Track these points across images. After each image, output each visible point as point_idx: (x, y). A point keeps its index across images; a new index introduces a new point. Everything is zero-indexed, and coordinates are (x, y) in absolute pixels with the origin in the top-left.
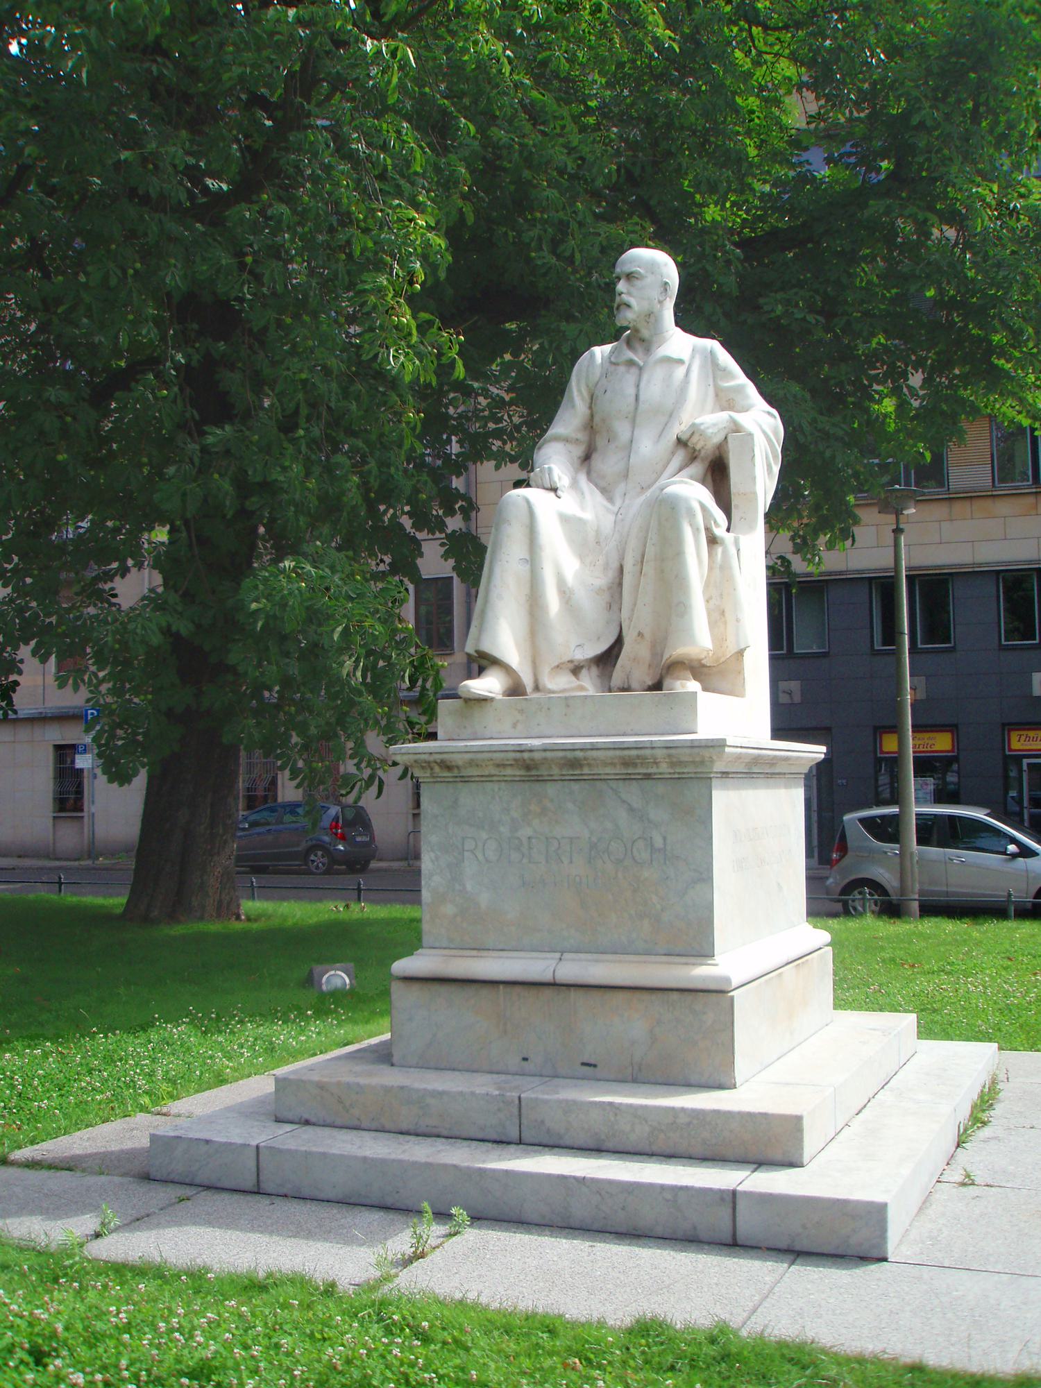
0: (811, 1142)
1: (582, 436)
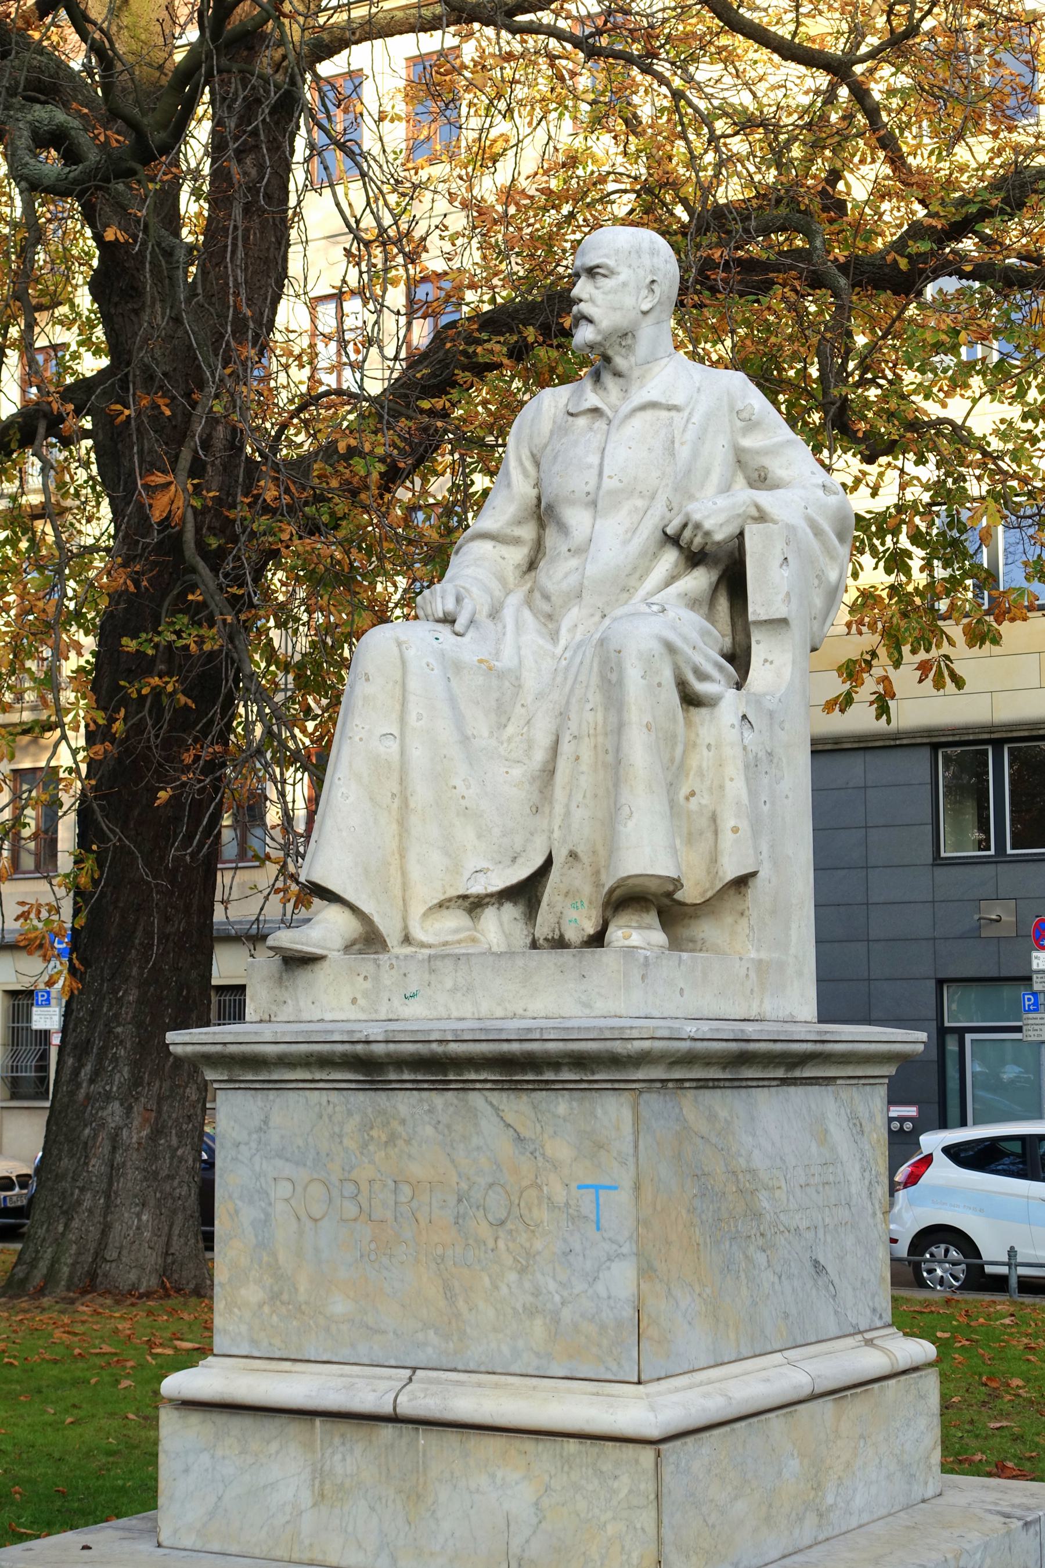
0: (684, 881)
1: (527, 532)
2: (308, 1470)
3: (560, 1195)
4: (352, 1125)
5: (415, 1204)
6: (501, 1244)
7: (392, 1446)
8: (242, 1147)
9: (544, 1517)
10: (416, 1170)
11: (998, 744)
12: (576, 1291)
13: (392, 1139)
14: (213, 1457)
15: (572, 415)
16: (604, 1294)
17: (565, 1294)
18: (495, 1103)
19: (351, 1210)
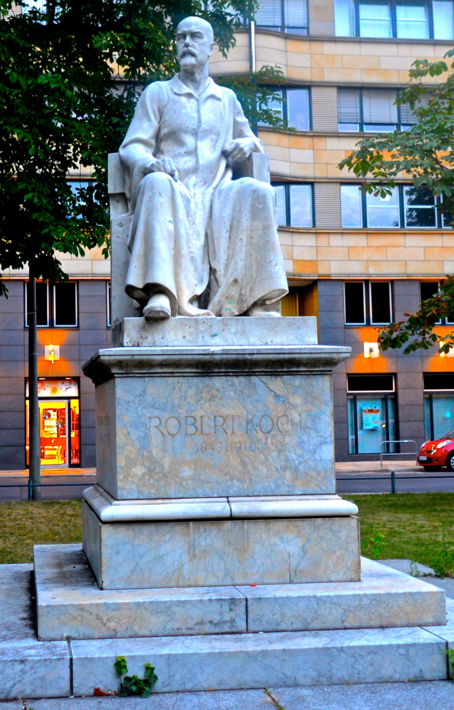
1: (153, 142)
2: (186, 545)
3: (297, 418)
4: (191, 392)
5: (225, 426)
6: (269, 441)
7: (231, 530)
8: (131, 404)
9: (307, 552)
10: (225, 411)
11: (367, 281)
12: (306, 458)
13: (213, 398)
14: (133, 545)
15: (178, 95)
16: (318, 458)
17: (301, 460)
18: (264, 381)
19: (191, 430)
